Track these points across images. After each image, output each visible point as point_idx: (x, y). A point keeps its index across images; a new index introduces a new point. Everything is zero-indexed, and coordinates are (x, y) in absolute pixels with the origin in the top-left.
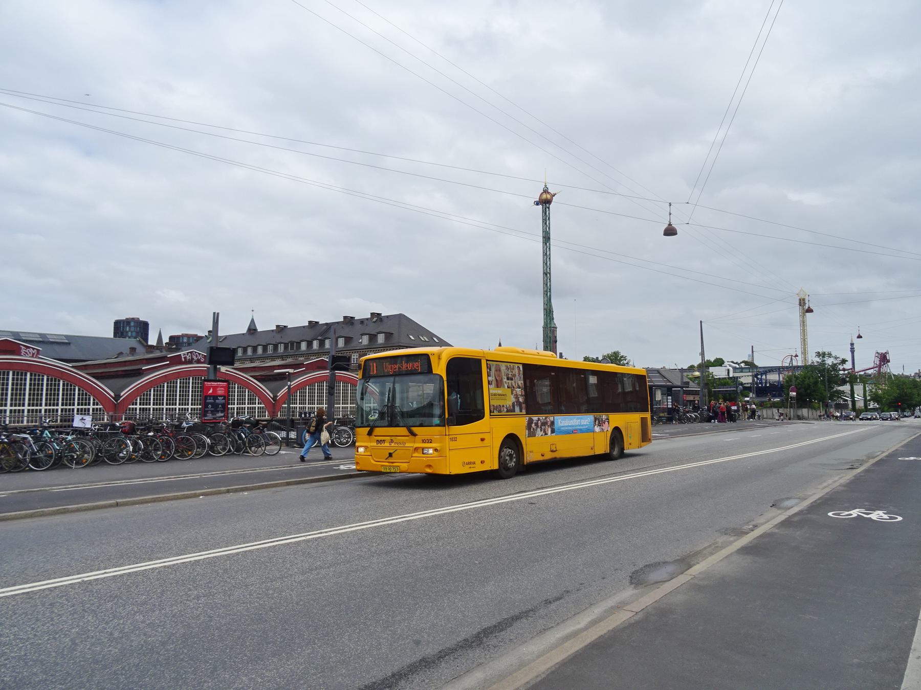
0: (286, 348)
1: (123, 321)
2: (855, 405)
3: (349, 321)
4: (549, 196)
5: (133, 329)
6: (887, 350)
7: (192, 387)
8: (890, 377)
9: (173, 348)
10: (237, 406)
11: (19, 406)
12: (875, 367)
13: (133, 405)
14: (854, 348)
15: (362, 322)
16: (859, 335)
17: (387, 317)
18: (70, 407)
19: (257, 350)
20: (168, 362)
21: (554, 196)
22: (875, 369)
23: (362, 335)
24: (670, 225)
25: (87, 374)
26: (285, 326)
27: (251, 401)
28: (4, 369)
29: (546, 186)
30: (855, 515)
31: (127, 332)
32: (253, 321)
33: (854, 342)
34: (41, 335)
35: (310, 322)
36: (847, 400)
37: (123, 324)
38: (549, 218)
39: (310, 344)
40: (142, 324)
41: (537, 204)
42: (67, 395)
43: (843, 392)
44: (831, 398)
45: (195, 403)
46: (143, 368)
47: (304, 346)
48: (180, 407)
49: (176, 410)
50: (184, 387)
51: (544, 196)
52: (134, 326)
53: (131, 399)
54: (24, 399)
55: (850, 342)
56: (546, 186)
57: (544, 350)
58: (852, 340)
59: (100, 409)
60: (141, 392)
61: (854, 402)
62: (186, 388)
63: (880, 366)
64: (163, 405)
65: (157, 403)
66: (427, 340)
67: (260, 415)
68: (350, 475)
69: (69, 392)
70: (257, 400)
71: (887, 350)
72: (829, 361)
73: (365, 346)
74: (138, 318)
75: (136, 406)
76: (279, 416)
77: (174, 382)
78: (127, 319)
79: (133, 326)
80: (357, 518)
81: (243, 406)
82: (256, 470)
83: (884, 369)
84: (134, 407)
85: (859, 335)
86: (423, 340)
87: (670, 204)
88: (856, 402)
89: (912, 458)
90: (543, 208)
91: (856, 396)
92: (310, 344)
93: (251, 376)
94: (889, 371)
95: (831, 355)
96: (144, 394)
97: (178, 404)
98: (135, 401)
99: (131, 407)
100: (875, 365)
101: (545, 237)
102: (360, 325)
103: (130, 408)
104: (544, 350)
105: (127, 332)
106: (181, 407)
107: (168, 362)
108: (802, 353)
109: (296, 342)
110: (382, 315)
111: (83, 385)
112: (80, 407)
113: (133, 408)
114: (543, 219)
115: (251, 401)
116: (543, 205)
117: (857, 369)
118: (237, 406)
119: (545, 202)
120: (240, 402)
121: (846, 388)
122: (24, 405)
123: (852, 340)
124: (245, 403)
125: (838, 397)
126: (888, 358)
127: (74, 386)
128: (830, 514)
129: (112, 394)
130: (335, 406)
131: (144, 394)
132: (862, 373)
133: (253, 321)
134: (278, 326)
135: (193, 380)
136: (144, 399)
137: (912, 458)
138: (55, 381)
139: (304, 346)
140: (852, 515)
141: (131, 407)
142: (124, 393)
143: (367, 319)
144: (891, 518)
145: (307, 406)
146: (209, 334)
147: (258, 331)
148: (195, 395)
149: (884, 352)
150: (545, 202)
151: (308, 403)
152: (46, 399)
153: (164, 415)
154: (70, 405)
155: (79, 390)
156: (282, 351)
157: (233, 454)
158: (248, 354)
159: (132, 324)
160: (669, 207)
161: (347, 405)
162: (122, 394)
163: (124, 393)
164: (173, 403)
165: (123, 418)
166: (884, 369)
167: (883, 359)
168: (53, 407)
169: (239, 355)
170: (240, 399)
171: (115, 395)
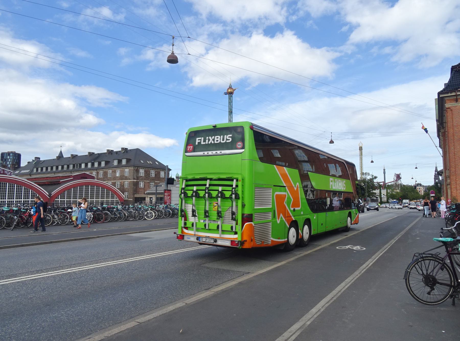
0: (74, 167)
1: (6, 153)
2: (382, 200)
3: (110, 152)
4: (232, 91)
6: (400, 173)
7: (90, 192)
8: (401, 186)
9: (16, 167)
10: (24, 200)
11: (3, 199)
12: (394, 181)
14: (385, 172)
15: (117, 152)
16: (372, 161)
17: (130, 150)
18: (20, 200)
19: (53, 168)
20: (72, 178)
21: (235, 90)
22: (394, 182)
23: (114, 160)
25: (35, 183)
26: (76, 155)
28: (11, 182)
30: (347, 248)
31: (8, 159)
32: (61, 152)
33: (385, 169)
35: (89, 153)
36: (377, 198)
37: (6, 155)
38: (232, 102)
39: (86, 165)
41: (226, 94)
42: (26, 194)
43: (375, 193)
44: (369, 196)
45: (91, 198)
46: (61, 181)
47: (83, 166)
49: (65, 201)
50: (81, 191)
51: (229, 90)
53: (56, 196)
54: (14, 196)
55: (383, 169)
57: (435, 99)
58: (384, 168)
59: (118, 200)
60: (61, 193)
61: (381, 198)
62: (80, 194)
63: (396, 181)
64: (65, 199)
66: (151, 163)
68: (89, 238)
69: (19, 192)
70: (115, 196)
71: (400, 173)
72: (369, 177)
73: (115, 166)
74: (15, 152)
75: (58, 200)
78: (8, 152)
79: (12, 156)
80: (91, 264)
81: (61, 200)
83: (399, 182)
85: (372, 161)
86: (149, 163)
87: (331, 133)
88: (382, 198)
91: (382, 195)
92: (86, 165)
95: (369, 174)
99: (56, 200)
100: (394, 180)
101: (230, 111)
102: (116, 154)
103: (55, 200)
104: (435, 99)
105: (8, 159)
107: (72, 178)
108: (360, 174)
109: (79, 164)
110: (128, 149)
111: (32, 188)
112: (9, 200)
113: (57, 200)
114: (229, 102)
115: (113, 197)
117: (386, 182)
118: (24, 200)
121: (377, 191)
122: (5, 199)
123: (384, 168)
125: (373, 196)
126: (400, 177)
127: (29, 190)
128: (337, 248)
129: (48, 194)
130: (87, 200)
132: (389, 184)
133: (61, 152)
134: (72, 155)
138: (20, 187)
139: (83, 166)
142: (53, 193)
143: (120, 151)
144: (361, 249)
145: (110, 199)
146: (35, 159)
147: (64, 157)
148: (80, 194)
149: (398, 173)
151: (111, 198)
152: (8, 196)
153: (66, 204)
154: (12, 199)
156: (71, 169)
157: (60, 225)
158: (48, 171)
159: (11, 155)
160: (436, 148)
161: (98, 200)
166: (399, 182)
167: (398, 177)
168: (27, 200)
169: (48, 171)
171: (49, 194)
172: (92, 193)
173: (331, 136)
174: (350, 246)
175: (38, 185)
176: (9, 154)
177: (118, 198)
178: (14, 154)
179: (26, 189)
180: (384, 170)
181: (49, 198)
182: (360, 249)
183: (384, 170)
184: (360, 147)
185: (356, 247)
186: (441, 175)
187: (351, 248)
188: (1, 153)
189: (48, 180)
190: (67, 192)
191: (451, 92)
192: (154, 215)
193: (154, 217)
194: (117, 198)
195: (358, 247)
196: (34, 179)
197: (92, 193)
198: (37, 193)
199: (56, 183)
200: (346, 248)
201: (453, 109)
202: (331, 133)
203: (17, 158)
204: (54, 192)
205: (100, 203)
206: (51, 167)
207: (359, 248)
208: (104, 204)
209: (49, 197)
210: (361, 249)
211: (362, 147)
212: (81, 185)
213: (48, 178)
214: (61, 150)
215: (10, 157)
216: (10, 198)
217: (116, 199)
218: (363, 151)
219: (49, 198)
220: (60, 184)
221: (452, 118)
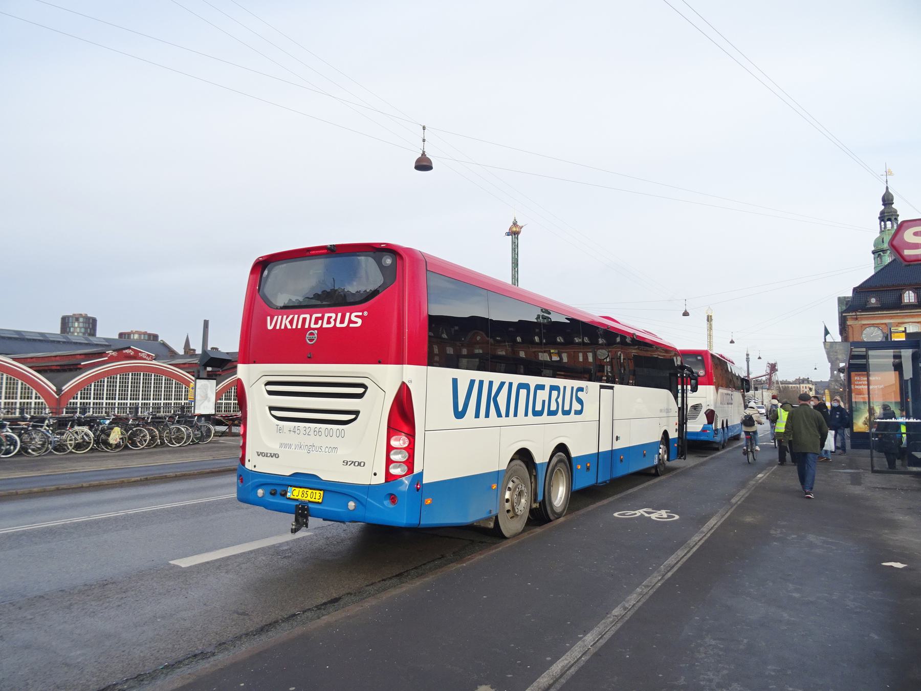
5: (81, 325)
7: (140, 384)
13: (74, 399)
16: (686, 311)
24: (423, 154)
25: (30, 367)
27: (26, 395)
29: (515, 220)
30: (638, 514)
34: (42, 334)
40: (91, 320)
41: (508, 235)
46: (82, 364)
48: (107, 401)
50: (112, 385)
51: (514, 229)
52: (83, 322)
53: (72, 393)
56: (515, 220)
59: (42, 403)
60: (83, 387)
63: (770, 374)
65: (133, 398)
67: (166, 411)
70: (184, 388)
74: (86, 314)
76: (140, 412)
77: (114, 377)
82: (76, 470)
84: (75, 401)
85: (686, 311)
89: (765, 443)
90: (512, 238)
93: (187, 372)
94: (777, 379)
96: (85, 389)
97: (163, 399)
98: (75, 396)
99: (72, 401)
103: (71, 403)
106: (95, 401)
115: (26, 395)
116: (512, 236)
119: (514, 233)
120: (156, 398)
124: (182, 398)
128: (616, 515)
129: (54, 388)
131: (85, 389)
135: (132, 375)
136: (84, 393)
137: (765, 443)
140: (636, 514)
141: (72, 401)
144: (669, 517)
149: (773, 363)
150: (514, 233)
153: (116, 409)
155: (22, 384)
159: (81, 320)
162: (63, 388)
163: (66, 388)
164: (87, 397)
165: (64, 412)
167: (773, 368)
170: (177, 394)
172: (156, 388)
173: (424, 141)
174: (645, 510)
175: (35, 371)
176: (76, 318)
177: (41, 397)
178: (86, 318)
179: (178, 385)
180: (748, 355)
181: (57, 397)
182: (666, 516)
183: (748, 355)
184: (708, 316)
185: (659, 512)
186: (843, 373)
187: (646, 515)
188: (61, 317)
189: (57, 361)
190: (95, 385)
191: (852, 312)
192: (148, 437)
193: (185, 442)
194: (39, 397)
195: (664, 513)
196: (54, 358)
197: (147, 389)
198: (33, 388)
199: (74, 368)
200: (636, 514)
201: (852, 326)
202: (424, 128)
203: (91, 327)
204: (71, 384)
205: (80, 408)
206: (600, 388)
207: (665, 516)
208: (25, 410)
209: (58, 395)
210: (669, 517)
211: (711, 316)
212: (124, 371)
213: (57, 358)
214: (887, 188)
215: (78, 325)
216: (110, 398)
217: (37, 401)
218: (713, 323)
219: (57, 397)
220: (80, 369)
221: (853, 334)
